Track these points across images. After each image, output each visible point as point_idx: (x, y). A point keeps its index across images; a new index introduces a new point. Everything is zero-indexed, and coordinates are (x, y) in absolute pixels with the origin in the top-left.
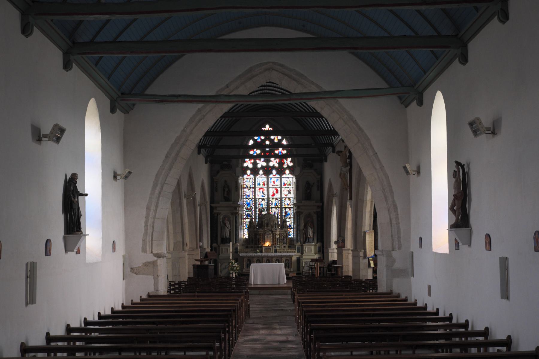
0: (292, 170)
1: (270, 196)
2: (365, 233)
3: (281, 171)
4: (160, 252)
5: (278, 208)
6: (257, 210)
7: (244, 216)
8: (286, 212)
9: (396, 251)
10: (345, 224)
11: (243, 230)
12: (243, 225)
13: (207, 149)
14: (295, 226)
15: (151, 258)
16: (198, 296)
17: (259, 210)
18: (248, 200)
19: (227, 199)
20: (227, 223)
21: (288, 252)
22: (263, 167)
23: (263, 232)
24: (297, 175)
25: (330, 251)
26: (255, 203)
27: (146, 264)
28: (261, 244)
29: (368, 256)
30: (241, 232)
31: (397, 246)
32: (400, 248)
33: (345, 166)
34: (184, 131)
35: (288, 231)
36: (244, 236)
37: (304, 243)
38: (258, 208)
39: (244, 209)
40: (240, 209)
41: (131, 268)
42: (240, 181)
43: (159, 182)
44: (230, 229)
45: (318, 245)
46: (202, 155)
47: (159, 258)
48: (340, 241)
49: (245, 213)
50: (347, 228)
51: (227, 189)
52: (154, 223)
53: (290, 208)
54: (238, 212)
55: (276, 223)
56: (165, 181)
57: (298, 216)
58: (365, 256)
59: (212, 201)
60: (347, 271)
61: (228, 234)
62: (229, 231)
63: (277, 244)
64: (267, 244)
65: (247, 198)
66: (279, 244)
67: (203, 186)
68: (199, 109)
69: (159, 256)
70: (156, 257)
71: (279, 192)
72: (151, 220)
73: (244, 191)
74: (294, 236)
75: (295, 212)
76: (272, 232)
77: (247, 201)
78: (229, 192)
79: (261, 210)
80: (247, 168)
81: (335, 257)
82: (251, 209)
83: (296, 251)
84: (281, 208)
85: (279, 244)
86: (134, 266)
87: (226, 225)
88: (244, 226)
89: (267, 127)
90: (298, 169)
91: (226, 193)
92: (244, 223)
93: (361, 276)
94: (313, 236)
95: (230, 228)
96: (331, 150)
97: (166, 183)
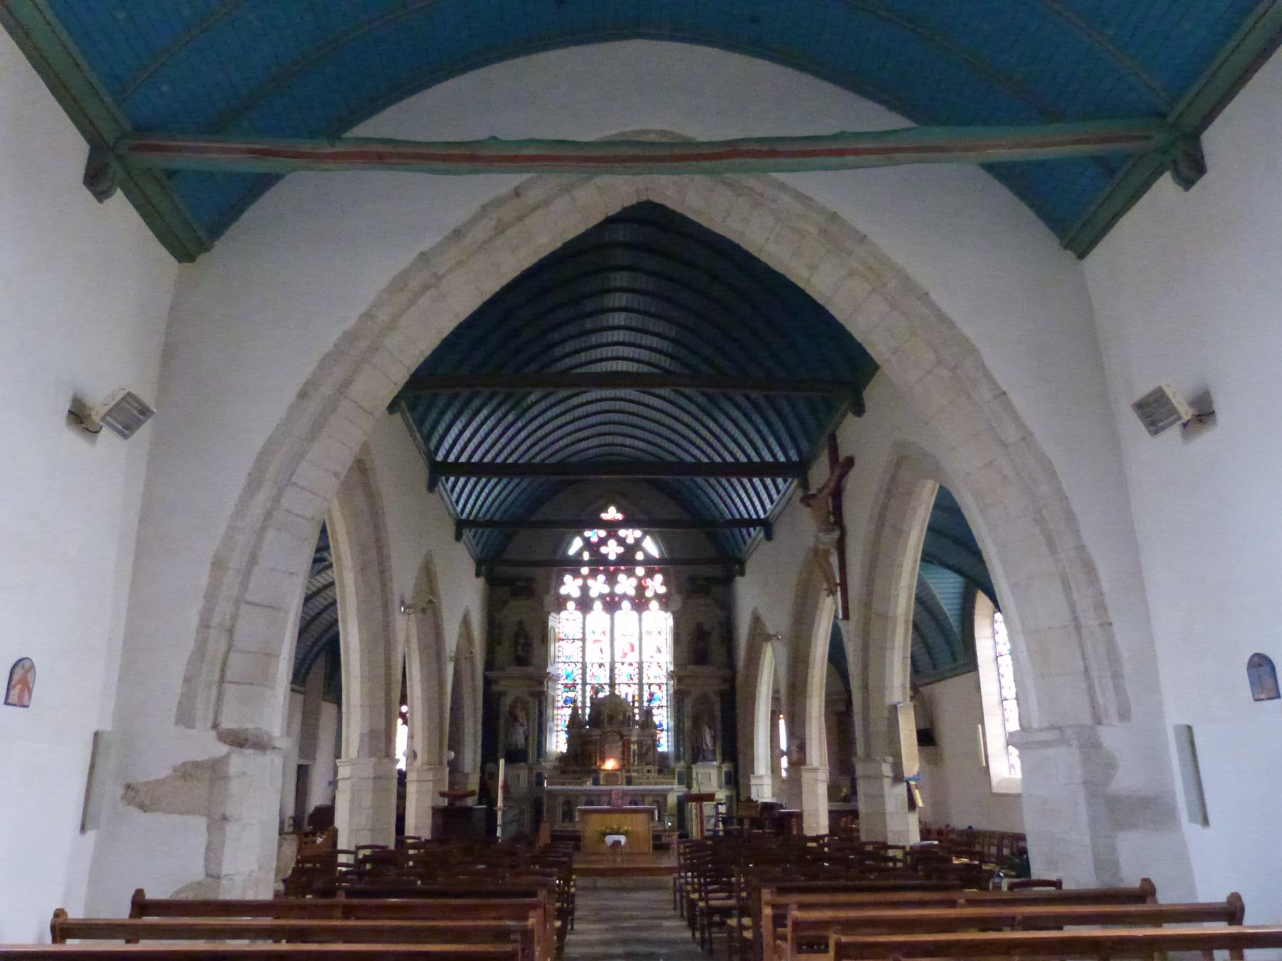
0: (665, 601)
1: (617, 658)
2: (894, 708)
3: (640, 603)
4: (250, 726)
5: (634, 684)
6: (588, 688)
7: (558, 701)
8: (651, 695)
9: (1110, 725)
10: (804, 709)
11: (555, 734)
12: (556, 722)
13: (480, 531)
14: (672, 724)
15: (206, 746)
16: (348, 912)
17: (592, 688)
18: (569, 665)
19: (522, 661)
20: (521, 714)
21: (656, 784)
22: (602, 597)
23: (601, 736)
24: (674, 609)
25: (753, 781)
26: (584, 674)
27: (188, 772)
28: (596, 764)
29: (907, 775)
30: (551, 738)
31: (1113, 710)
32: (1124, 715)
33: (828, 531)
34: (368, 316)
35: (657, 733)
36: (557, 747)
37: (695, 761)
38: (590, 684)
39: (560, 686)
40: (550, 683)
41: (128, 787)
42: (551, 623)
43: (268, 476)
44: (527, 730)
45: (726, 767)
46: (465, 543)
47: (239, 750)
48: (794, 748)
49: (560, 694)
50: (810, 714)
51: (522, 641)
52: (234, 618)
53: (659, 685)
54: (545, 689)
55: (629, 716)
56: (292, 475)
57: (679, 698)
58: (898, 777)
59: (489, 665)
60: (814, 825)
61: (520, 740)
62: (524, 733)
63: (633, 765)
64: (610, 764)
65: (565, 663)
66: (636, 763)
67: (466, 622)
68: (422, 254)
69: (238, 740)
70: (225, 742)
71: (637, 648)
72: (224, 608)
73: (559, 647)
74: (670, 749)
75: (671, 691)
76: (622, 736)
77: (566, 669)
78: (528, 645)
79: (596, 691)
80: (568, 598)
81: (765, 796)
82: (574, 685)
83: (676, 781)
84: (641, 685)
85: (636, 763)
86: (140, 777)
87: (518, 721)
88: (557, 726)
89: (612, 514)
90: (677, 602)
91: (519, 648)
92: (559, 717)
93: (889, 834)
94: (714, 743)
95: (526, 727)
96: (762, 535)
97: (295, 484)
